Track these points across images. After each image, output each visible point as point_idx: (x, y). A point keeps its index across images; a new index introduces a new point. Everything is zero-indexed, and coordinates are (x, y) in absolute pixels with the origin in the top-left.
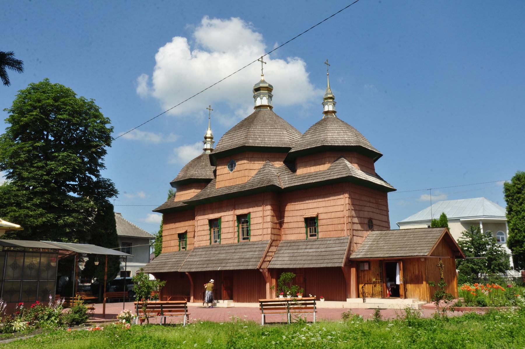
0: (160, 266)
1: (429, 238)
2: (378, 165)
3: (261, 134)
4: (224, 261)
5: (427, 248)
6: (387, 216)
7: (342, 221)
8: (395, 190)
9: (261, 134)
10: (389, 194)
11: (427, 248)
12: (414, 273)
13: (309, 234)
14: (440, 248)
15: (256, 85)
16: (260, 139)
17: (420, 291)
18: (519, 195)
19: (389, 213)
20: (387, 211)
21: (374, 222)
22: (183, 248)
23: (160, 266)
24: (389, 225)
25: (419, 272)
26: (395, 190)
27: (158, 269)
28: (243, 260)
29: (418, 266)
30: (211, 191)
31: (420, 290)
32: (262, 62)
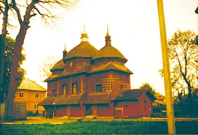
2: (127, 65)
10: (131, 75)
21: (123, 86)
26: (133, 74)
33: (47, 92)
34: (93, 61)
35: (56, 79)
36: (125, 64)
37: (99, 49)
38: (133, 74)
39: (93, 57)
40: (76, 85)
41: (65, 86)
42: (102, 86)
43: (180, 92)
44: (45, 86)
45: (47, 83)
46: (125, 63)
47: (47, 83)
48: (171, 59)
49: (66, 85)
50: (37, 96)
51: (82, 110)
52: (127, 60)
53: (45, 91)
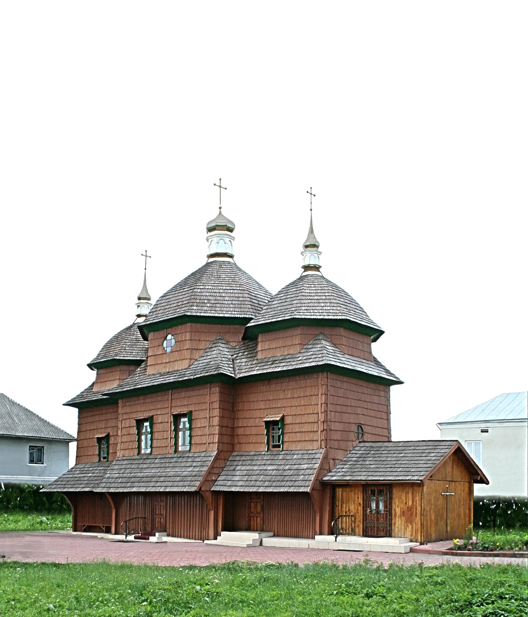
0: (72, 483)
1: (432, 455)
2: (378, 349)
3: (211, 298)
4: (154, 479)
5: (425, 469)
6: (388, 420)
7: (315, 427)
8: (64, 405)
9: (211, 298)
10: (393, 388)
11: (425, 469)
12: (406, 503)
13: (271, 443)
14: (449, 469)
15: (208, 223)
16: (208, 305)
17: (412, 528)
18: (521, 602)
19: (391, 415)
20: (388, 413)
21: (365, 428)
22: (104, 458)
23: (72, 483)
24: (389, 433)
25: (413, 502)
26: (401, 383)
27: (69, 486)
28: (178, 479)
29: (413, 493)
30: (142, 380)
31: (412, 526)
32: (220, 187)
33: (73, 446)
34: (249, 334)
35: (112, 400)
36: (373, 344)
37: (274, 292)
38: (401, 383)
39: (252, 319)
40: (151, 427)
41: (147, 424)
42: (287, 429)
43: (478, 542)
44: (68, 422)
45: (76, 410)
46: (375, 340)
47: (76, 410)
48: (149, 299)
49: (189, 415)
50: (37, 456)
51: (212, 513)
52: (382, 333)
53: (66, 442)
